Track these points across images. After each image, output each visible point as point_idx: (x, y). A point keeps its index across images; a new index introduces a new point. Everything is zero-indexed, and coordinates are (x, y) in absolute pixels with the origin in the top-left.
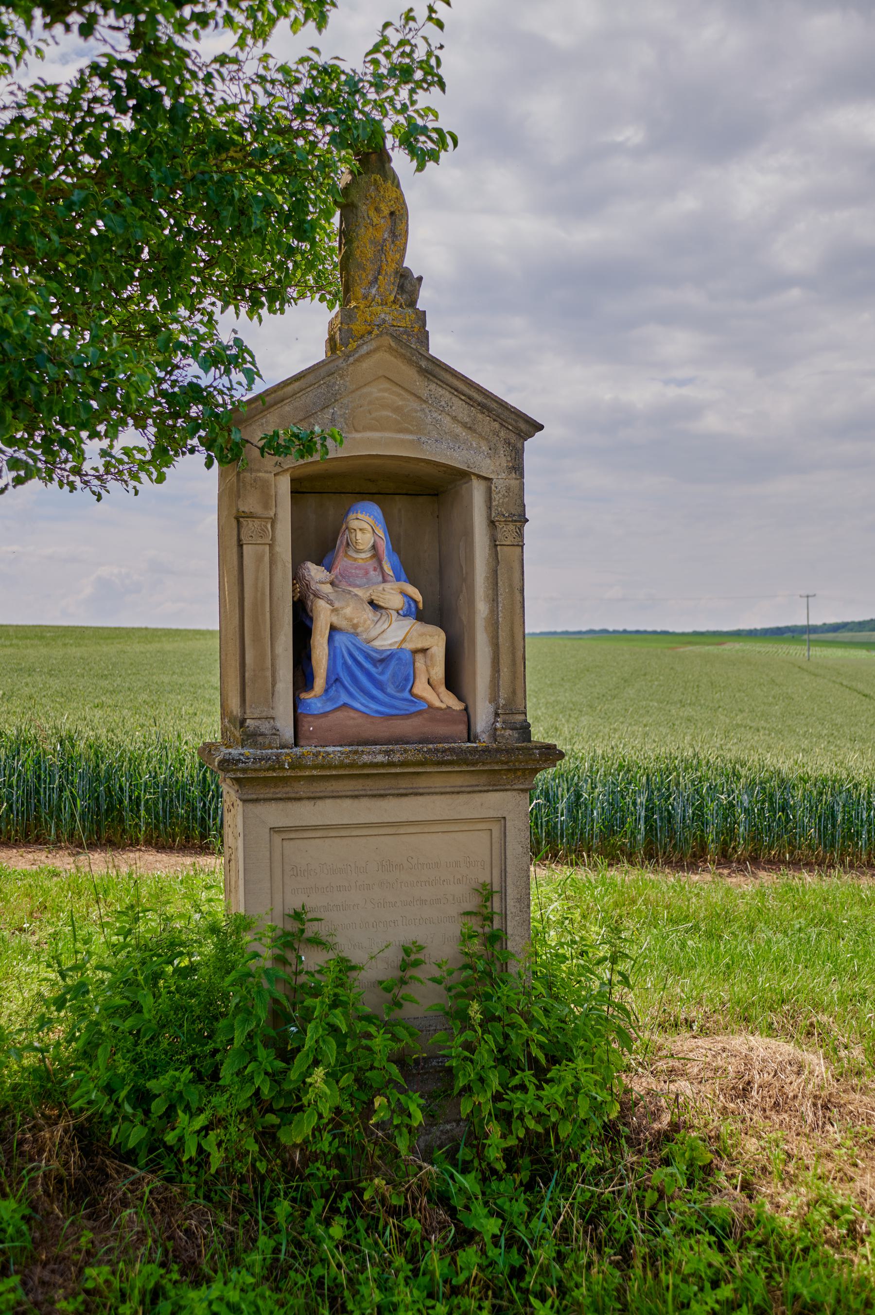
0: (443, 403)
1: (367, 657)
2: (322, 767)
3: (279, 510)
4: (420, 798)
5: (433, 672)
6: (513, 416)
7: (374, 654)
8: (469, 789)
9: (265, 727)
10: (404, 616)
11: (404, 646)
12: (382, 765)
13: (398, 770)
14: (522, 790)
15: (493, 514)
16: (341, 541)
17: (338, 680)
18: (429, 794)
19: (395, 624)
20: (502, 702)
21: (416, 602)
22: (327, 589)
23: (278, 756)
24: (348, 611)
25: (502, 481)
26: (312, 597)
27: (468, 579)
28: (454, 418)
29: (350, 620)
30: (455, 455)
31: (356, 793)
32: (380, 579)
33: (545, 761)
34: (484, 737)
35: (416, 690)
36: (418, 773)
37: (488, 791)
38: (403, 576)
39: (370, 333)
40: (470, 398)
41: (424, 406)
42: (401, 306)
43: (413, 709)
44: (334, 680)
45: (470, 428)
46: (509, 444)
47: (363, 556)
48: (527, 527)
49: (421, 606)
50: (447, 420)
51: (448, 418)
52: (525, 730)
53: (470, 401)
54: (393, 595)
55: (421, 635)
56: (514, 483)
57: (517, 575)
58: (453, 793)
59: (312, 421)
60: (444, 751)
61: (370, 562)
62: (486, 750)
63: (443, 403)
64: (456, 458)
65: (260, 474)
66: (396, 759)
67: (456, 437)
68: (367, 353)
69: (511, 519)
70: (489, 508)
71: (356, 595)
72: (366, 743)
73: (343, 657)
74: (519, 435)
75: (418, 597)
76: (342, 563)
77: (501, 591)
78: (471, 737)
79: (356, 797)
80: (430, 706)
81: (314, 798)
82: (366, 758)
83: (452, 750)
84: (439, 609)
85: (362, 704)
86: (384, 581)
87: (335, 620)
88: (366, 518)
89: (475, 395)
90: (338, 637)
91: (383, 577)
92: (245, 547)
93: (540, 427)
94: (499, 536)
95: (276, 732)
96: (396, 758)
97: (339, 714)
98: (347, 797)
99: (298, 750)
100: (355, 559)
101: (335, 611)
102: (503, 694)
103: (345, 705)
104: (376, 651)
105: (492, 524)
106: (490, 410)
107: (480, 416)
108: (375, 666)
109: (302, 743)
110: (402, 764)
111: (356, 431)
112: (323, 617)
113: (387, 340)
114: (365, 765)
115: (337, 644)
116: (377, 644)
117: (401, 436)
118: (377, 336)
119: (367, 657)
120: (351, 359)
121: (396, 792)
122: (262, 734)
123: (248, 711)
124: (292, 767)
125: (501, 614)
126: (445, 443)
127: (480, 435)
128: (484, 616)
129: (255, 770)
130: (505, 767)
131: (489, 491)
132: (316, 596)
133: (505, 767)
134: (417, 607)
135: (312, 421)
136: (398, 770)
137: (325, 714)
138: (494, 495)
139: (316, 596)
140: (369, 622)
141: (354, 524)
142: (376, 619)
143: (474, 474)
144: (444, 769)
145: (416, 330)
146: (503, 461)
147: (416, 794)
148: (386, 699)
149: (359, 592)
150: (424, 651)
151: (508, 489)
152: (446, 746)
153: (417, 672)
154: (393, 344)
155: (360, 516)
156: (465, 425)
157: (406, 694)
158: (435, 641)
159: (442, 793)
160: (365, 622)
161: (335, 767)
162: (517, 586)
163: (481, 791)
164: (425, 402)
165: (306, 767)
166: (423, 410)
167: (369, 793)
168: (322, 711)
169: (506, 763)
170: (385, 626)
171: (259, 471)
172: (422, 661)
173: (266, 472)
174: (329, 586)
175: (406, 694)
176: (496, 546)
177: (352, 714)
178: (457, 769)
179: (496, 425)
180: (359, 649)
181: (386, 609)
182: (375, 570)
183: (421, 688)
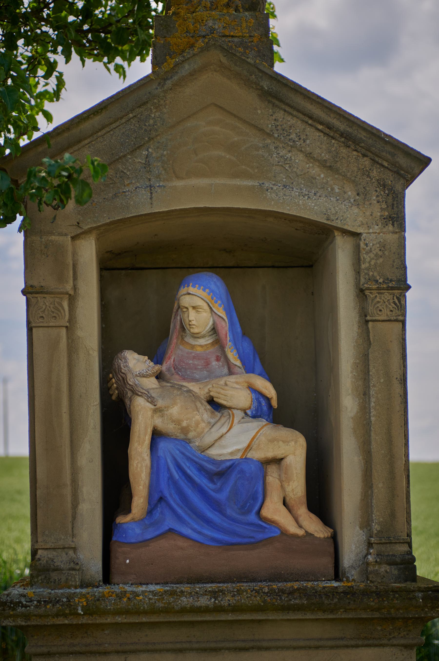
0: (293, 136)
1: (201, 469)
2: (127, 612)
3: (81, 284)
4: (265, 654)
5: (289, 489)
6: (388, 148)
7: (209, 466)
8: (330, 643)
9: (61, 560)
10: (254, 417)
11: (249, 455)
12: (206, 610)
13: (230, 617)
14: (406, 646)
15: (362, 280)
16: (175, 326)
17: (161, 499)
18: (277, 648)
19: (236, 428)
20: (376, 527)
21: (268, 400)
22: (151, 383)
23: (70, 597)
24: (175, 411)
25: (374, 235)
26: (129, 394)
27: (333, 368)
28: (309, 156)
29: (178, 422)
30: (311, 204)
31: (178, 646)
32: (226, 370)
33: (433, 608)
34: (354, 574)
35: (265, 512)
36: (260, 621)
37: (357, 646)
38: (258, 367)
39: (192, 46)
40: (329, 127)
41: (268, 141)
42: (236, 10)
43: (260, 536)
44: (156, 501)
45: (330, 168)
46: (384, 186)
47: (202, 342)
48: (409, 294)
49: (275, 403)
50: (299, 159)
51: (301, 156)
52: (408, 564)
53: (329, 131)
54: (237, 391)
55: (272, 441)
56: (391, 238)
57: (396, 359)
58: (310, 648)
59: (120, 167)
60: (292, 592)
61: (211, 349)
62: (349, 593)
63: (293, 136)
64: (311, 207)
65: (53, 238)
66: (225, 603)
67: (311, 181)
68: (191, 74)
69: (388, 284)
70: (358, 272)
71: (189, 391)
72: (200, 580)
73: (169, 469)
74: (398, 173)
75: (269, 390)
76: (176, 352)
77: (373, 381)
78: (337, 574)
79: (181, 651)
80: (284, 533)
81: (124, 652)
82: (185, 601)
83: (302, 591)
84: (301, 407)
85: (194, 530)
86: (231, 373)
87: (159, 422)
88: (200, 292)
89: (336, 123)
90: (162, 445)
91: (229, 368)
92: (34, 330)
93: (427, 161)
94: (371, 309)
95: (76, 566)
96: (226, 600)
97: (164, 543)
98: (168, 650)
99: (105, 589)
100: (193, 347)
101: (157, 411)
102: (377, 516)
103: (171, 530)
104: (213, 461)
105: (361, 293)
106: (356, 142)
107: (344, 151)
108: (212, 481)
109: (115, 578)
110: (235, 609)
111: (179, 178)
112: (143, 419)
113: (216, 56)
114: (183, 611)
115: (161, 453)
116: (214, 452)
117: (238, 182)
118: (202, 50)
119: (201, 469)
120: (169, 83)
121: (231, 645)
122: (57, 569)
123: (40, 540)
124: (88, 612)
125: (373, 412)
126: (304, 195)
127: (345, 176)
128: (352, 414)
129: (40, 616)
130: (377, 615)
131: (357, 250)
132: (135, 393)
133: (377, 615)
134: (270, 406)
135: (120, 167)
136: (230, 617)
137: (146, 542)
138: (363, 255)
139: (135, 393)
140: (203, 425)
141: (186, 301)
142: (213, 421)
143: (338, 229)
144: (292, 616)
145: (255, 40)
146: (377, 210)
147: (260, 649)
148: (226, 524)
149: (194, 387)
150: (278, 461)
151: (383, 246)
152: (296, 585)
153: (269, 488)
154: (224, 60)
155: (191, 290)
156: (323, 164)
157: (252, 517)
158: (293, 448)
159: (295, 648)
160: (197, 424)
161: (145, 613)
162: (396, 372)
163: (347, 647)
164: (270, 135)
165: (105, 613)
166: (266, 147)
167: (195, 646)
168: (140, 539)
169: (378, 610)
170: (224, 430)
171: (52, 233)
172: (276, 475)
173: (61, 234)
174: (153, 379)
175: (252, 517)
176: (367, 322)
177: (181, 543)
178: (309, 616)
179: (366, 162)
180: (189, 459)
181: (230, 408)
182: (218, 360)
183: (273, 510)
